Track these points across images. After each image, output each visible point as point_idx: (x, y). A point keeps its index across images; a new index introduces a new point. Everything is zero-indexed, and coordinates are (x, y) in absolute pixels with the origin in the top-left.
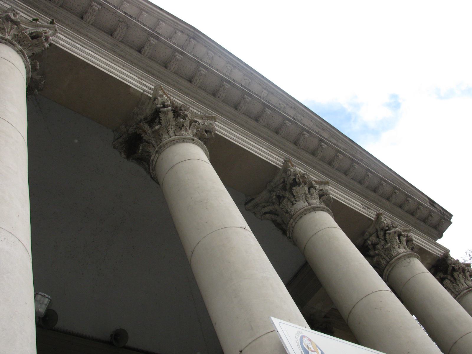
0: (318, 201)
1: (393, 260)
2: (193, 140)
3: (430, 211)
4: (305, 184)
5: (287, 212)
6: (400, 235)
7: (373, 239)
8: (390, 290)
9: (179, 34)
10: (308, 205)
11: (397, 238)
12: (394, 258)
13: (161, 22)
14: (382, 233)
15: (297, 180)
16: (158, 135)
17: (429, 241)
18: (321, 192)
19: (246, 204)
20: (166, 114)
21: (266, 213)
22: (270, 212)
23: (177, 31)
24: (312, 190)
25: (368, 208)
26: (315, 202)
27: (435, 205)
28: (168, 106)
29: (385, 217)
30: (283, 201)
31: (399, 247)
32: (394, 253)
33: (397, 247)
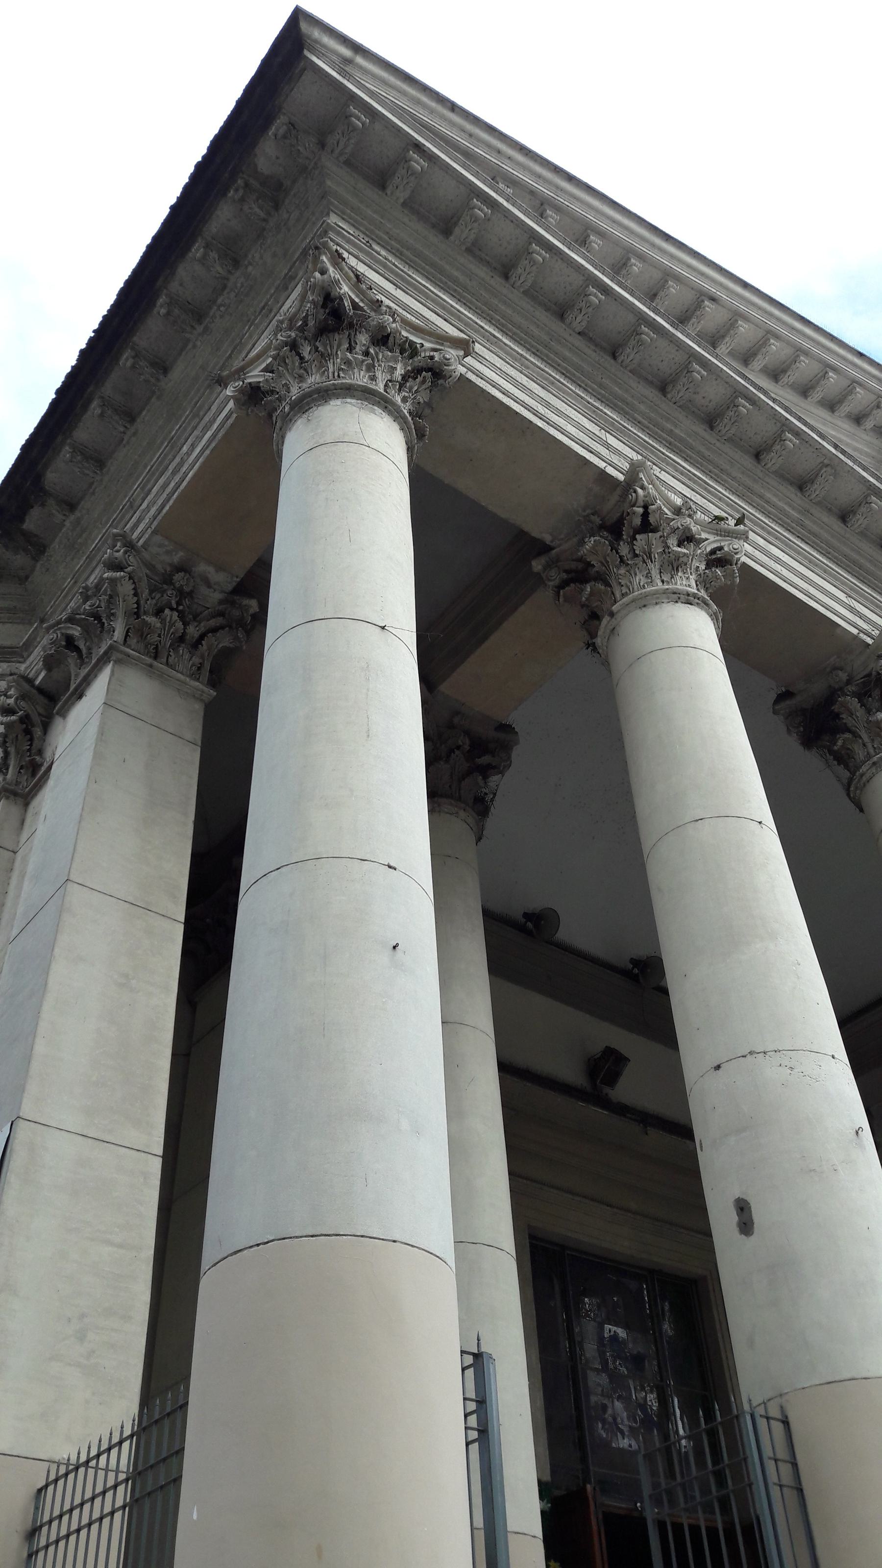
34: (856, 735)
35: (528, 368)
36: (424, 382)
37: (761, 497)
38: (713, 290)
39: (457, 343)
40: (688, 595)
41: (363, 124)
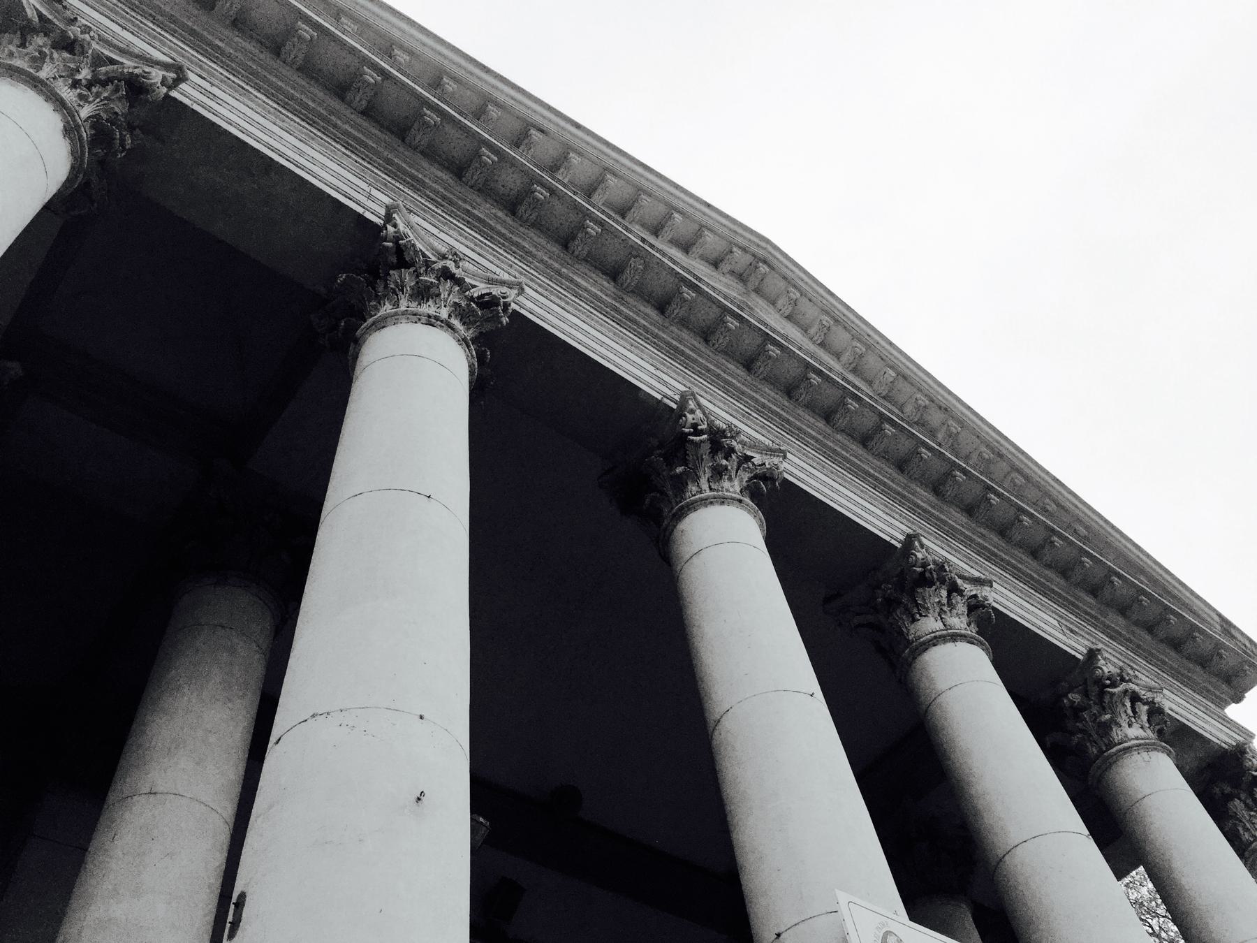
0: (965, 619)
1: (1114, 750)
2: (740, 501)
3: (1219, 645)
4: (943, 582)
5: (901, 633)
6: (1135, 698)
7: (1075, 697)
8: (1087, 832)
9: (737, 252)
10: (942, 627)
11: (1128, 704)
12: (1116, 745)
13: (706, 232)
14: (1096, 689)
15: (927, 575)
16: (680, 484)
17: (1207, 711)
18: (973, 601)
19: (827, 600)
20: (697, 445)
21: (860, 626)
22: (870, 625)
23: (735, 249)
24: (957, 599)
25: (1072, 631)
26: (959, 621)
27: (1233, 631)
28: (700, 433)
29: (1105, 659)
30: (895, 610)
31: (1130, 725)
32: (1117, 734)
33: (1125, 725)
34: (663, 493)
35: (164, 44)
36: (117, 90)
37: (572, 281)
38: (540, 120)
39: (510, 285)
40: (429, 317)
41: (312, 37)
